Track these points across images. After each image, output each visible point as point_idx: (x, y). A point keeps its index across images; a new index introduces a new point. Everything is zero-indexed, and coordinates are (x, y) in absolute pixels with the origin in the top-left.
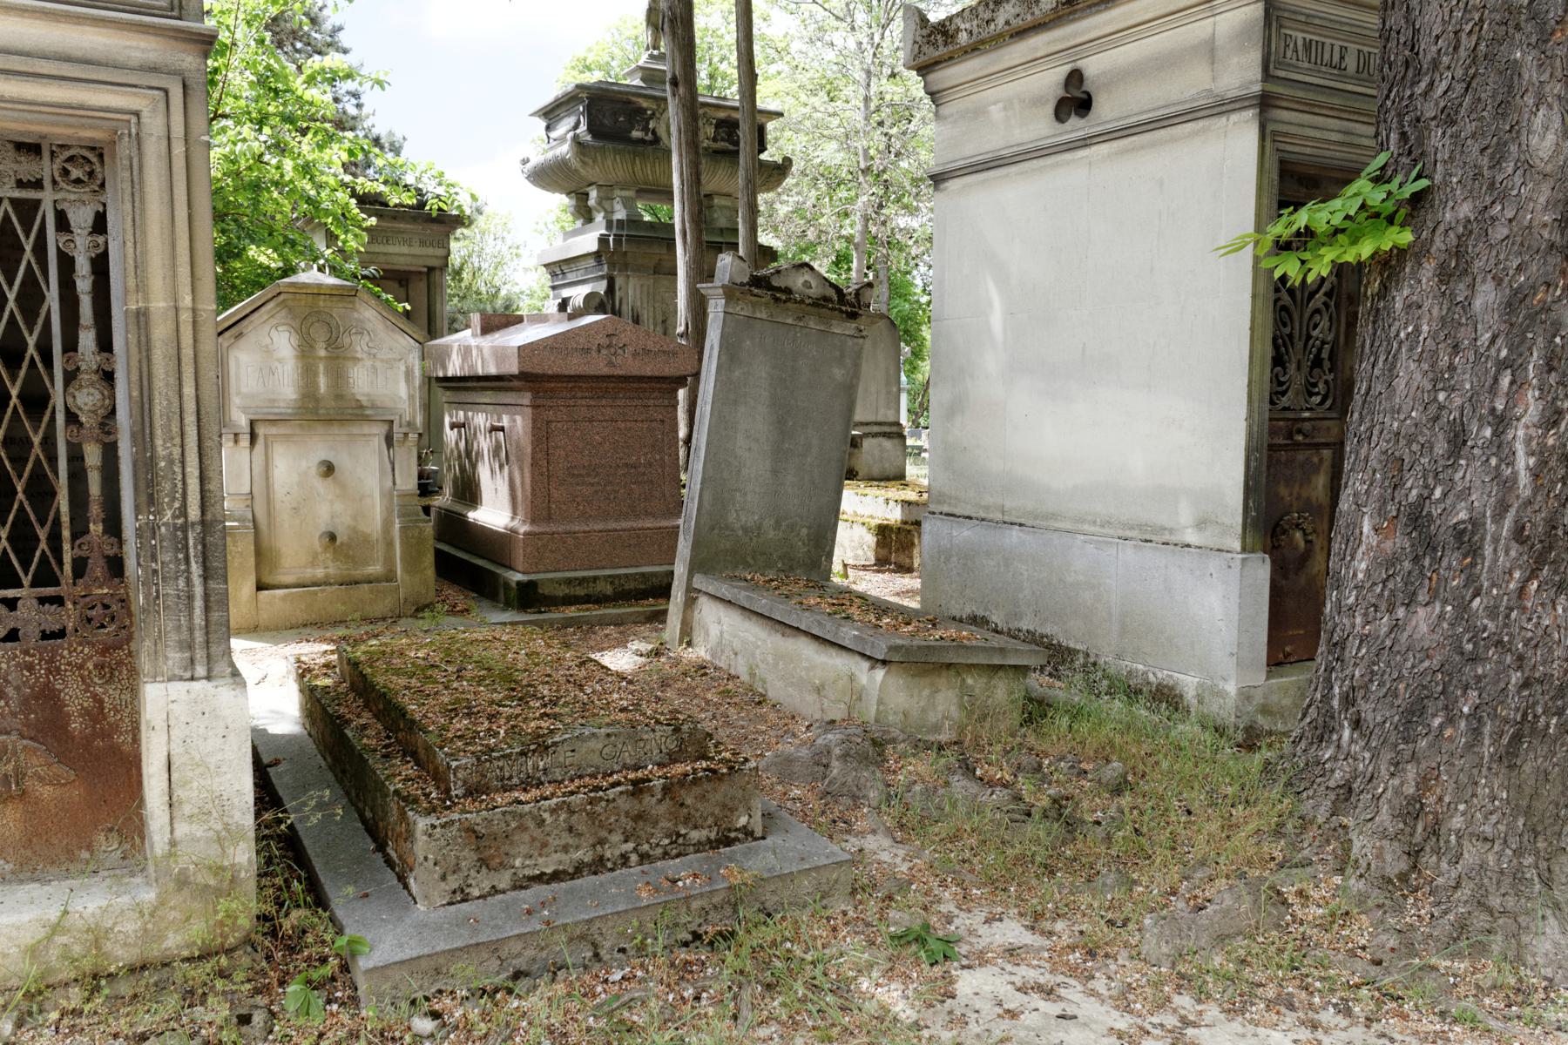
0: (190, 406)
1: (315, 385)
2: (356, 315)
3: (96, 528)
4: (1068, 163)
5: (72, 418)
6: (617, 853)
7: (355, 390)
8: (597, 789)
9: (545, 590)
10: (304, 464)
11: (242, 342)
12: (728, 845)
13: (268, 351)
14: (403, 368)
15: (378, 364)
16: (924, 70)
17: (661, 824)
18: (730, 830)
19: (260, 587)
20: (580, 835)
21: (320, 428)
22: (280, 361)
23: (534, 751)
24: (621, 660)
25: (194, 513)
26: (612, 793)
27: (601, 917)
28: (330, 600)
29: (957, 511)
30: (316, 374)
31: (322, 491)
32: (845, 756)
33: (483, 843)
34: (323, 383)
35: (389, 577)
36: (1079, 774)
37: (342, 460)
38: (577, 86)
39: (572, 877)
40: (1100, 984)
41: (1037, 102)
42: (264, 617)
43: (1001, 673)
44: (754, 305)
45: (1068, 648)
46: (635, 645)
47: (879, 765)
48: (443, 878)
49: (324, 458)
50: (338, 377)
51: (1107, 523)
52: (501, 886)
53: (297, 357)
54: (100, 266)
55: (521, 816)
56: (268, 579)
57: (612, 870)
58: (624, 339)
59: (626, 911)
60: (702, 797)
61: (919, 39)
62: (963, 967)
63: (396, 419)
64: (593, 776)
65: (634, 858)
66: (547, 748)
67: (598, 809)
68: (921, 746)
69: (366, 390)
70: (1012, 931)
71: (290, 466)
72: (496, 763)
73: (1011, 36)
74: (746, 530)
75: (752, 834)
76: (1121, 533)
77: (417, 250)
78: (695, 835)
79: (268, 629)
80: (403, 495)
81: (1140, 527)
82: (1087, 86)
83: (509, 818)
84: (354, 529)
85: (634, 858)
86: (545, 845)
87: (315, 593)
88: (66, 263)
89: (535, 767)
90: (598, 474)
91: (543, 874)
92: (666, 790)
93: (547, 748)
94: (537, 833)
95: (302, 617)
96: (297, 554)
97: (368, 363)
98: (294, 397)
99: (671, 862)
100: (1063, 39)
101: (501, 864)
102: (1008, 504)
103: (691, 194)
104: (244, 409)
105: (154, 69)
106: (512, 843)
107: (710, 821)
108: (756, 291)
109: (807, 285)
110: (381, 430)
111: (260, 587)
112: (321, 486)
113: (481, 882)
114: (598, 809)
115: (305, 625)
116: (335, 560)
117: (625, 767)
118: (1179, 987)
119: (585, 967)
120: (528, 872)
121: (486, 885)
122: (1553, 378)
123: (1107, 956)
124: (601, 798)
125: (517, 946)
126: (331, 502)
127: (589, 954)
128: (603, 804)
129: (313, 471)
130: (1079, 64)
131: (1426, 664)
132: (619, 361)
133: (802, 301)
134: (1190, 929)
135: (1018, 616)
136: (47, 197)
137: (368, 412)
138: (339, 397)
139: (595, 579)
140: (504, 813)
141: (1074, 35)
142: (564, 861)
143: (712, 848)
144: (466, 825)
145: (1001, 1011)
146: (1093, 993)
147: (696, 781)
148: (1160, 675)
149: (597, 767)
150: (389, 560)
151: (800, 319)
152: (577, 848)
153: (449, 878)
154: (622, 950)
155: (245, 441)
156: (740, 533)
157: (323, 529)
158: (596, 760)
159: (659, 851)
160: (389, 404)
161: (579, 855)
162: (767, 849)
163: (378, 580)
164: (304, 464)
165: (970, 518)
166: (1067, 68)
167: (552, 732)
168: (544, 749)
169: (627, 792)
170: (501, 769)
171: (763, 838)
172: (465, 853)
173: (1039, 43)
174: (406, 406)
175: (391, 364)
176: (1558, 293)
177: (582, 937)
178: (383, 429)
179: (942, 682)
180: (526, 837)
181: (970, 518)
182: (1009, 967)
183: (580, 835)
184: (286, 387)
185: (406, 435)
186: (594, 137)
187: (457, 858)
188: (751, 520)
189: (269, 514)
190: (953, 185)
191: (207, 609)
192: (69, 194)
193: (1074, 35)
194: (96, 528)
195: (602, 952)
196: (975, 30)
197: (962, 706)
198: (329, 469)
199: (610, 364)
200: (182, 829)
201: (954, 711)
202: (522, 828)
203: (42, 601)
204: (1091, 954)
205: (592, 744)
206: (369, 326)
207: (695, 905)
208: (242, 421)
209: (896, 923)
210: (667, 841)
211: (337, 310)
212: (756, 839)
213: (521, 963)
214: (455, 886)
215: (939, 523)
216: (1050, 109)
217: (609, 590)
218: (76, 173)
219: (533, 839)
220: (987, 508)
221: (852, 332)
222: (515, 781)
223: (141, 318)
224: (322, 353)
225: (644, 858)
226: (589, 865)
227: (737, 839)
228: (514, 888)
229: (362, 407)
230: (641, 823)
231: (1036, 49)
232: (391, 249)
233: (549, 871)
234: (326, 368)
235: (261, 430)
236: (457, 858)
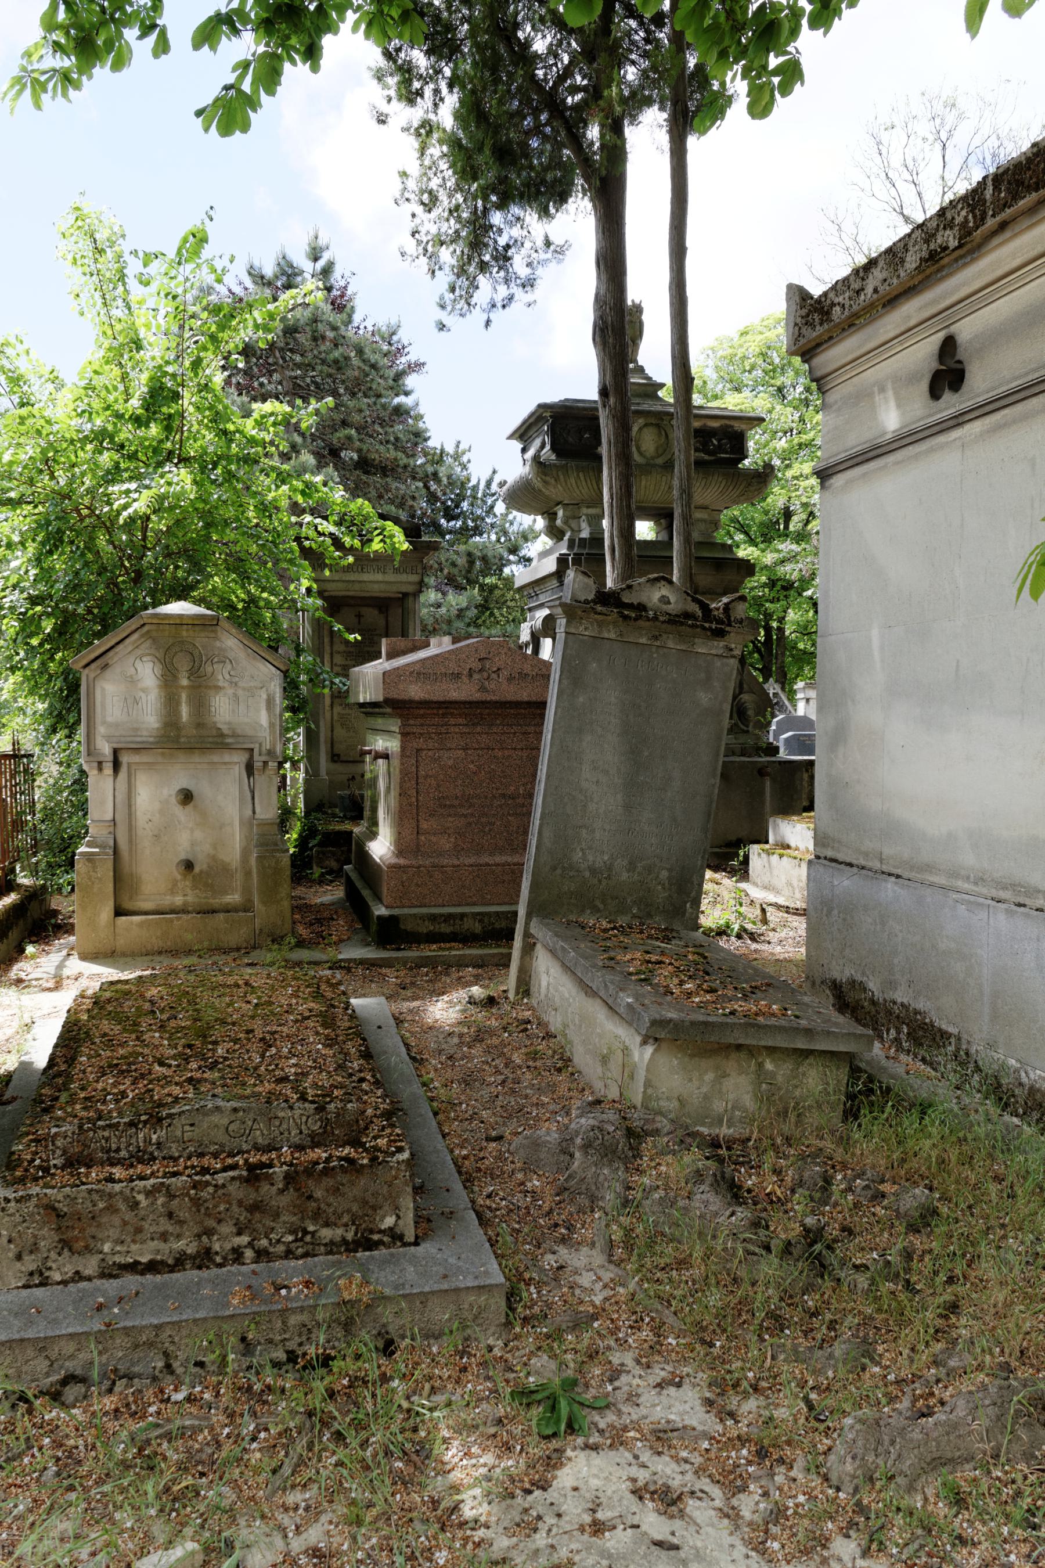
2: (218, 644)
4: (942, 447)
6: (228, 1246)
7: (217, 719)
8: (205, 1171)
9: (409, 926)
10: (165, 792)
11: (108, 673)
12: (369, 1249)
13: (132, 681)
14: (265, 696)
15: (240, 692)
16: (807, 353)
17: (283, 1218)
18: (372, 1232)
19: (119, 912)
20: (181, 1223)
22: (143, 690)
23: (145, 1122)
24: (444, 1011)
26: (220, 1178)
27: (173, 1323)
28: (185, 929)
29: (841, 857)
30: (178, 703)
31: (183, 819)
32: (586, 1147)
33: (65, 1223)
34: (185, 711)
35: (246, 907)
36: (874, 1198)
37: (203, 788)
38: (540, 406)
39: (172, 1269)
40: (750, 1505)
41: (912, 379)
42: (121, 943)
43: (811, 1060)
44: (600, 624)
45: (940, 1030)
46: (460, 995)
47: (626, 1161)
48: (19, 1257)
49: (178, 788)
50: (200, 705)
51: (980, 880)
52: (87, 1272)
53: (160, 687)
55: (111, 1196)
56: (127, 905)
57: (220, 1266)
59: (205, 1319)
60: (336, 1191)
61: (799, 320)
62: (587, 1447)
63: (256, 747)
64: (215, 1155)
65: (249, 1254)
66: (160, 1120)
67: (203, 1194)
68: (687, 1138)
69: (228, 718)
70: (685, 1407)
71: (151, 794)
72: (101, 1133)
73: (884, 306)
74: (593, 871)
75: (401, 1237)
76: (994, 893)
78: (326, 1234)
79: (124, 955)
80: (263, 824)
81: (1014, 886)
82: (961, 354)
83: (95, 1197)
84: (214, 858)
85: (249, 1254)
86: (139, 1230)
87: (171, 920)
89: (148, 1141)
90: (471, 806)
91: (137, 1263)
92: (289, 1178)
93: (160, 1120)
94: (129, 1216)
95: (157, 943)
96: (156, 882)
97: (230, 691)
98: (156, 725)
99: (293, 1263)
100: (934, 301)
101: (86, 1247)
102: (887, 851)
103: (620, 508)
104: (108, 738)
106: (99, 1226)
107: (346, 1218)
108: (599, 608)
109: (665, 600)
110: (242, 758)
111: (119, 912)
112: (178, 811)
113: (62, 1267)
114: (203, 1194)
115: (160, 953)
116: (194, 887)
117: (257, 1148)
118: (852, 1524)
119: (155, 1379)
120: (118, 1259)
121: (69, 1270)
123: (781, 1461)
124: (207, 1184)
125: (70, 1348)
126: (192, 830)
127: (160, 1364)
128: (211, 1189)
129: (173, 800)
130: (954, 329)
132: (492, 686)
133: (655, 618)
134: (893, 1442)
135: (892, 985)
137: (229, 740)
138: (199, 725)
139: (462, 916)
140: (90, 1191)
141: (943, 297)
142: (164, 1251)
143: (348, 1250)
144: (45, 1201)
145: (587, 1519)
146: (731, 1514)
147: (327, 1172)
148: (1032, 1076)
149: (222, 1145)
150: (246, 890)
151: (656, 638)
152: (179, 1237)
153: (26, 1258)
154: (200, 1364)
155: (108, 770)
156: (587, 874)
157: (183, 856)
158: (221, 1137)
159: (281, 1248)
160: (250, 732)
161: (181, 1244)
162: (414, 1260)
163: (236, 910)
164: (165, 792)
165: (851, 865)
166: (941, 336)
167: (177, 1100)
168: (156, 1121)
169: (239, 1178)
170: (107, 1139)
171: (416, 1244)
172: (45, 1232)
173: (911, 310)
174: (267, 734)
175: (251, 692)
177: (150, 1344)
178: (243, 758)
179: (730, 1065)
180: (116, 1220)
181: (851, 865)
182: (645, 1456)
183: (181, 1223)
184: (149, 717)
185: (265, 763)
186: (558, 456)
187: (35, 1236)
188: (600, 860)
189: (130, 841)
190: (838, 481)
193: (943, 297)
195: (176, 1365)
196: (847, 303)
197: (758, 1097)
198: (187, 797)
199: (483, 689)
201: (748, 1101)
202: (111, 1209)
204: (762, 1454)
205: (215, 1118)
206: (231, 655)
207: (294, 1320)
208: (105, 749)
209: (538, 1373)
210: (290, 1238)
211: (200, 640)
212: (405, 1245)
213: (73, 1366)
214: (32, 1267)
215: (821, 869)
216: (924, 385)
217: (477, 928)
219: (125, 1223)
220: (866, 854)
221: (720, 652)
222: (123, 1153)
224: (185, 682)
225: (261, 1255)
226: (193, 1258)
227: (380, 1243)
228: (103, 1275)
229: (222, 735)
230: (257, 1215)
231: (909, 317)
233: (144, 1260)
234: (189, 697)
236: (35, 1236)
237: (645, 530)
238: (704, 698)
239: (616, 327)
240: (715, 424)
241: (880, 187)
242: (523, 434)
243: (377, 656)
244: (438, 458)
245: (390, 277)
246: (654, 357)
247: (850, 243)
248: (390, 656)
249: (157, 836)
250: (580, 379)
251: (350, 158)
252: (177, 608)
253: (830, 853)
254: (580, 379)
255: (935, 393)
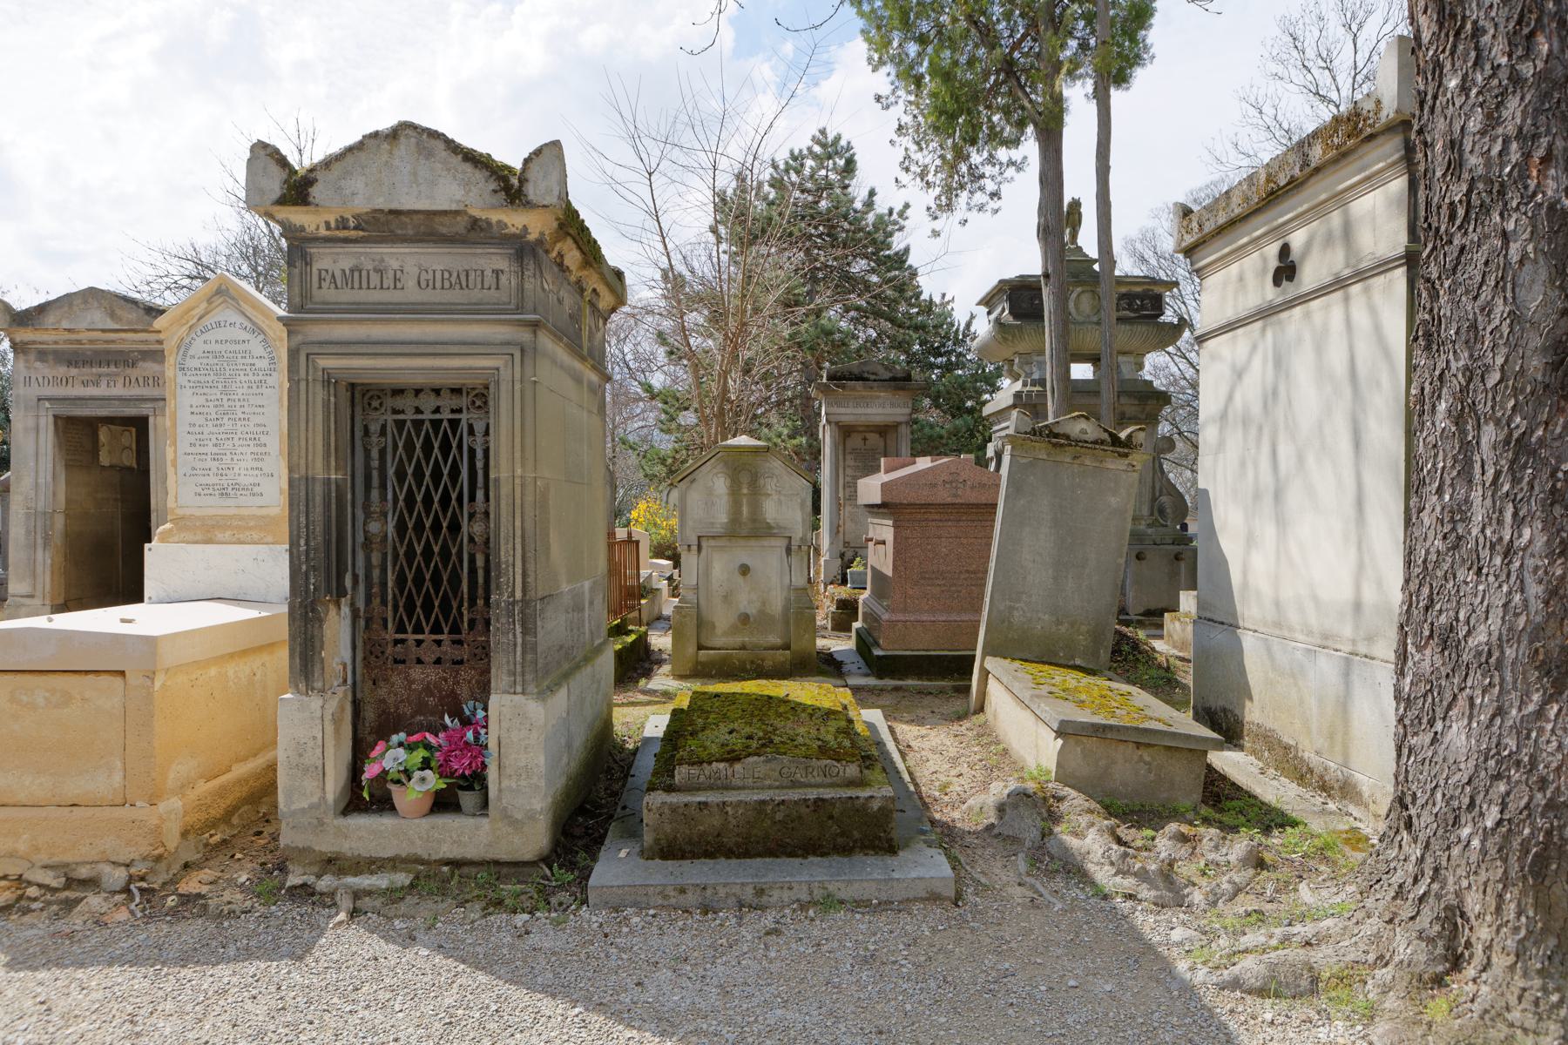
0: (518, 533)
1: (741, 513)
3: (480, 602)
5: (471, 539)
13: (710, 492)
21: (742, 542)
25: (518, 595)
29: (1216, 618)
38: (1001, 281)
50: (756, 507)
54: (486, 452)
56: (705, 643)
58: (964, 476)
77: (889, 410)
88: (472, 452)
97: (775, 497)
105: (508, 343)
109: (1084, 432)
110: (783, 543)
111: (700, 647)
112: (740, 579)
122: (1558, 511)
131: (1457, 777)
136: (464, 417)
138: (754, 521)
176: (1558, 430)
191: (524, 653)
192: (475, 414)
194: (480, 602)
200: (505, 783)
203: (454, 642)
218: (478, 403)
223: (497, 480)
224: (745, 491)
232: (869, 411)
235: (704, 544)
237: (1081, 371)
238: (1114, 501)
239: (1057, 219)
240: (1139, 289)
241: (1299, 76)
242: (988, 301)
243: (877, 469)
244: (929, 307)
245: (888, 166)
246: (1088, 240)
247: (1272, 124)
248: (887, 472)
249: (726, 597)
250: (1029, 260)
251: (861, 109)
252: (743, 440)
253: (1209, 615)
254: (1029, 260)
255: (1277, 282)
